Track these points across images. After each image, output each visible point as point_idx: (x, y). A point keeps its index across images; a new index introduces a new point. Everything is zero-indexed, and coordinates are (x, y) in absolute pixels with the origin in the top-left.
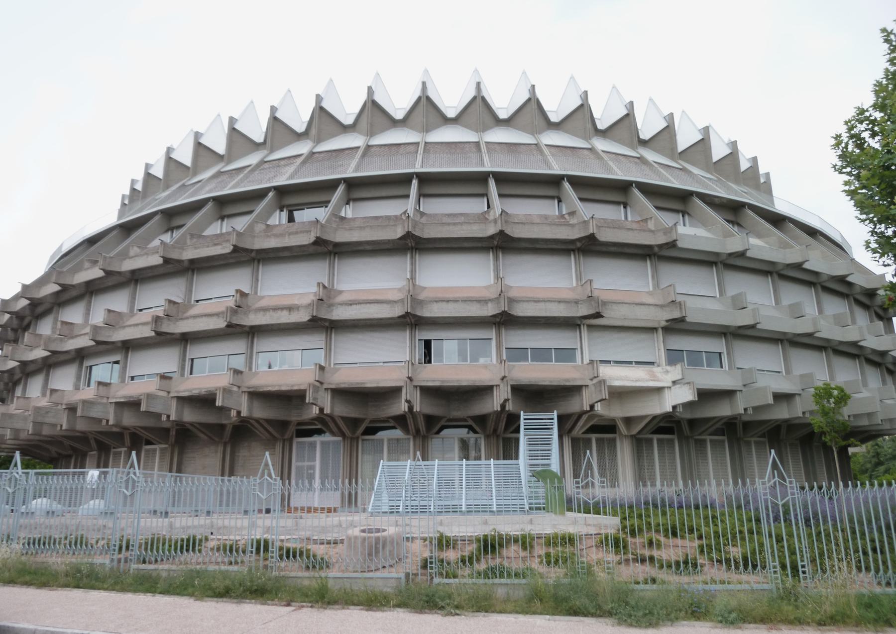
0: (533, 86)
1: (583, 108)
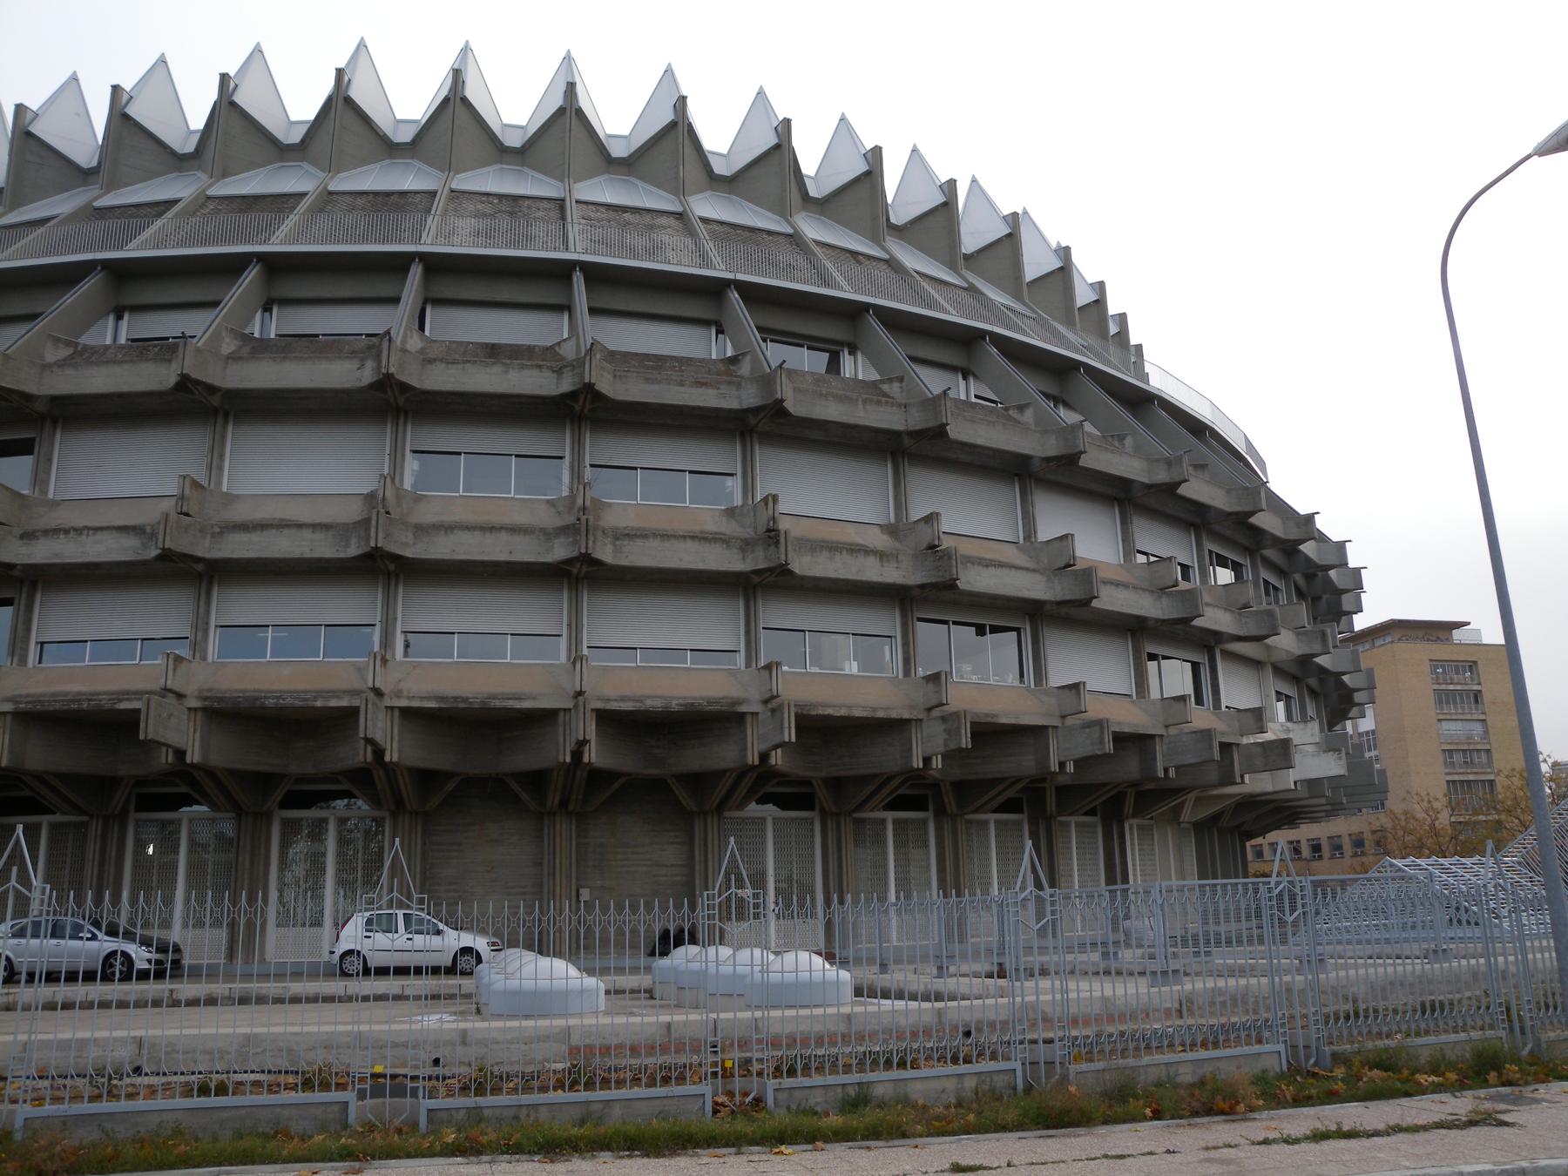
0: (683, 99)
1: (780, 152)
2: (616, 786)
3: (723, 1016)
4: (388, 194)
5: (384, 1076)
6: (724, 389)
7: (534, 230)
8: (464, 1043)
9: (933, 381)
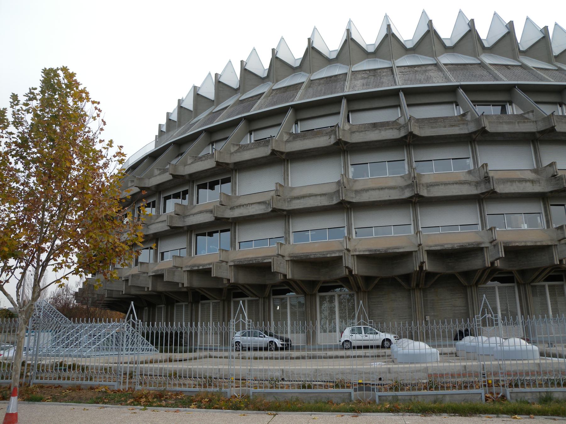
0: (431, 21)
1: (472, 32)
2: (436, 278)
3: (486, 363)
4: (331, 77)
5: (363, 384)
6: (461, 126)
7: (383, 80)
8: (390, 372)
9: (547, 110)
